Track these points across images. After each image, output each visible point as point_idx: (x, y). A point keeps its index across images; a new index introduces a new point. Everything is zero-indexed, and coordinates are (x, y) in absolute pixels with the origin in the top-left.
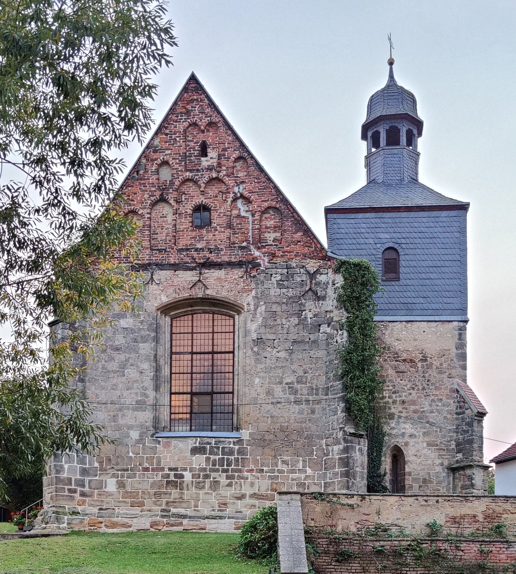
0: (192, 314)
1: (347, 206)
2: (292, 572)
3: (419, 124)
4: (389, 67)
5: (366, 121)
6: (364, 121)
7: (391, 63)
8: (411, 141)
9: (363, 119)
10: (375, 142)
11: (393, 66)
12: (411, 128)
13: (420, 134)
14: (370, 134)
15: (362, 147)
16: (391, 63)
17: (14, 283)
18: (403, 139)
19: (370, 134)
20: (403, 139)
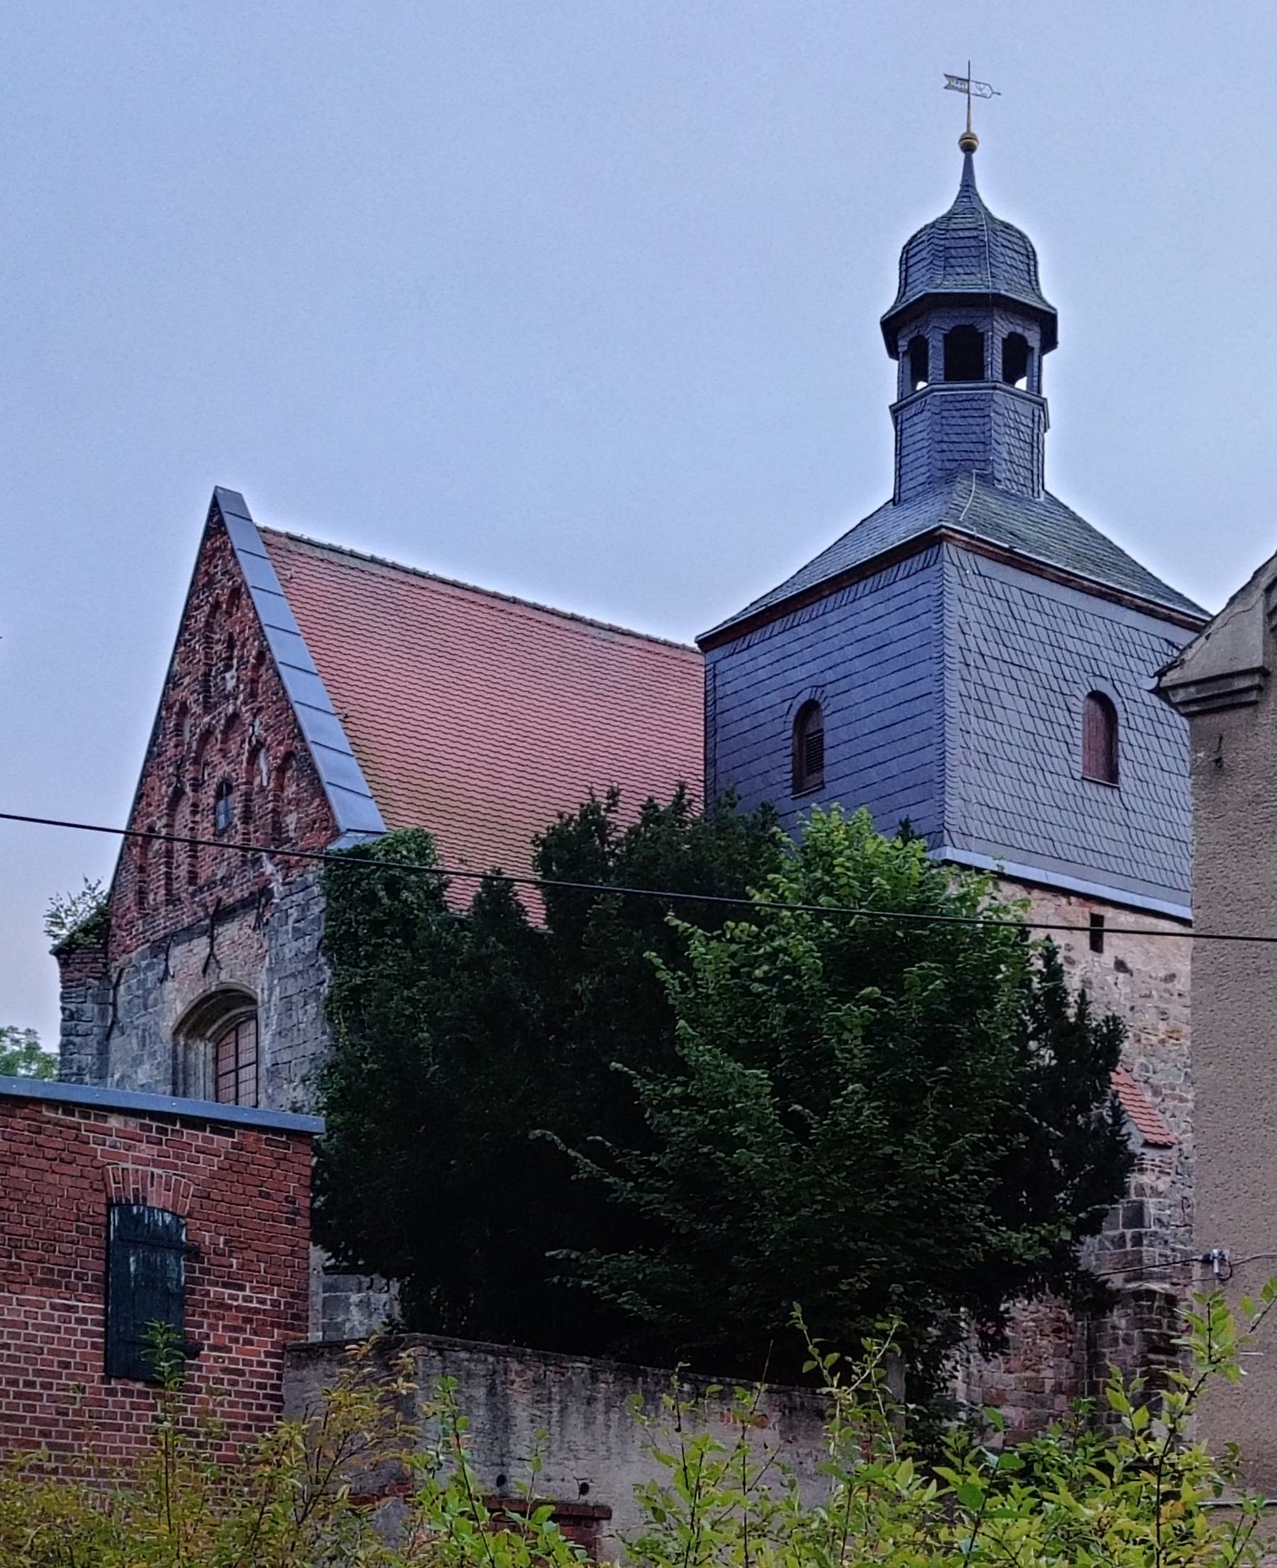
0: (704, 782)
1: (835, 568)
2: (942, 352)
3: (1047, 322)
4: (962, 156)
5: (898, 300)
6: (891, 303)
7: (968, 147)
8: (1019, 360)
9: (886, 298)
10: (915, 366)
11: (975, 156)
12: (1019, 330)
13: (1049, 342)
14: (903, 345)
15: (886, 374)
16: (968, 147)
17: (1150, 1420)
18: (995, 359)
19: (903, 345)
20: (995, 359)
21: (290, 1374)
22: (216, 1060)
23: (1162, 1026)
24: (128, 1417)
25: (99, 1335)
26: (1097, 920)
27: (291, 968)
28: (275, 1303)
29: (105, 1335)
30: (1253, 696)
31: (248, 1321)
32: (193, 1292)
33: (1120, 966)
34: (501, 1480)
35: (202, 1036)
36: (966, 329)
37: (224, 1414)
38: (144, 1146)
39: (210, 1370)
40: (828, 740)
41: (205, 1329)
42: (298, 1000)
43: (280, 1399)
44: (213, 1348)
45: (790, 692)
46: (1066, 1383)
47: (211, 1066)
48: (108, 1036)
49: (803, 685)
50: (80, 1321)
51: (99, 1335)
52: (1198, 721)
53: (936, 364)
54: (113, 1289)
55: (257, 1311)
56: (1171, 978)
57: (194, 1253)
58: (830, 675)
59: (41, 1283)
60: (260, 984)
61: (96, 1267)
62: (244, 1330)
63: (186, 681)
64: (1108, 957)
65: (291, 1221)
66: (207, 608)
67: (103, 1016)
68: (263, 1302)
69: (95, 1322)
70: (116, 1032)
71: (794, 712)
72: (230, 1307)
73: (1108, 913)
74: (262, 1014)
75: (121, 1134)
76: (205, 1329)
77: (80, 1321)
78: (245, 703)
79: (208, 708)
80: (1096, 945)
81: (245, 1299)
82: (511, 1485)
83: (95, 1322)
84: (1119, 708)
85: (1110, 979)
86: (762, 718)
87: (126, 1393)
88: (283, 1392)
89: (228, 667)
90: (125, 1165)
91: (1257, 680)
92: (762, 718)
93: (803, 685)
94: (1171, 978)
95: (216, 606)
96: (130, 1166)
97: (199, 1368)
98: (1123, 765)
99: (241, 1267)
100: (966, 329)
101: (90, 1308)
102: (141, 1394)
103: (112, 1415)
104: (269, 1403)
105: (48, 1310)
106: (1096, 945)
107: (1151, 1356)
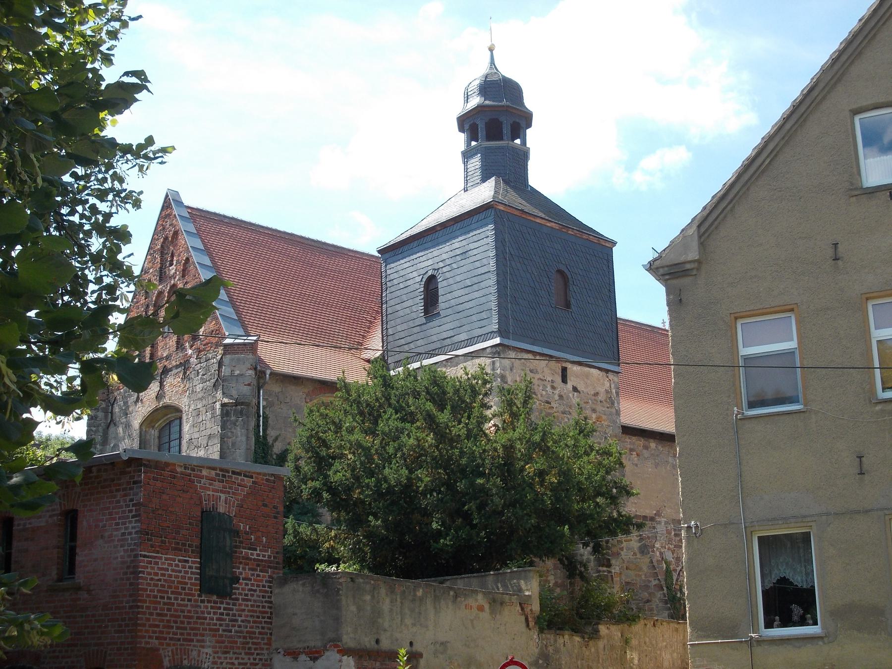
7: (491, 50)
16: (491, 50)
21: (276, 591)
22: (159, 437)
23: (594, 416)
24: (209, 613)
25: (197, 573)
26: (564, 370)
27: (200, 395)
28: (269, 557)
29: (200, 574)
30: (695, 272)
31: (258, 565)
32: (236, 552)
33: (575, 389)
34: (377, 641)
35: (153, 427)
36: (497, 122)
37: (249, 611)
38: (217, 483)
39: (243, 589)
40: (441, 292)
41: (241, 570)
42: (203, 410)
43: (271, 602)
44: (244, 579)
45: (423, 271)
46: (560, 581)
47: (157, 440)
48: (108, 427)
49: (430, 268)
50: (190, 567)
51: (197, 573)
52: (669, 282)
53: (481, 133)
54: (205, 553)
55: (262, 561)
56: (597, 394)
57: (237, 533)
58: (441, 265)
59: (175, 549)
60: (184, 403)
61: (197, 542)
62: (256, 570)
63: (151, 270)
64: (569, 386)
65: (275, 517)
66: (162, 240)
67: (106, 417)
68: (264, 556)
69: (196, 568)
70: (112, 425)
71: (424, 280)
72: (251, 559)
73: (569, 366)
74: (184, 417)
75: (208, 478)
76: (241, 570)
77: (190, 567)
78: (179, 280)
79: (161, 280)
80: (564, 380)
81: (258, 555)
82: (381, 644)
83: (196, 568)
84: (570, 277)
85: (571, 395)
86: (409, 283)
87: (209, 602)
88: (272, 599)
89: (171, 265)
90: (208, 493)
91: (696, 265)
92: (409, 283)
93: (430, 268)
94: (597, 394)
95: (166, 238)
96: (211, 493)
97: (238, 589)
98: (572, 301)
99: (256, 539)
100: (497, 122)
101: (194, 562)
102: (215, 602)
103: (203, 612)
104: (267, 605)
105: (177, 562)
106: (564, 380)
107: (601, 568)
